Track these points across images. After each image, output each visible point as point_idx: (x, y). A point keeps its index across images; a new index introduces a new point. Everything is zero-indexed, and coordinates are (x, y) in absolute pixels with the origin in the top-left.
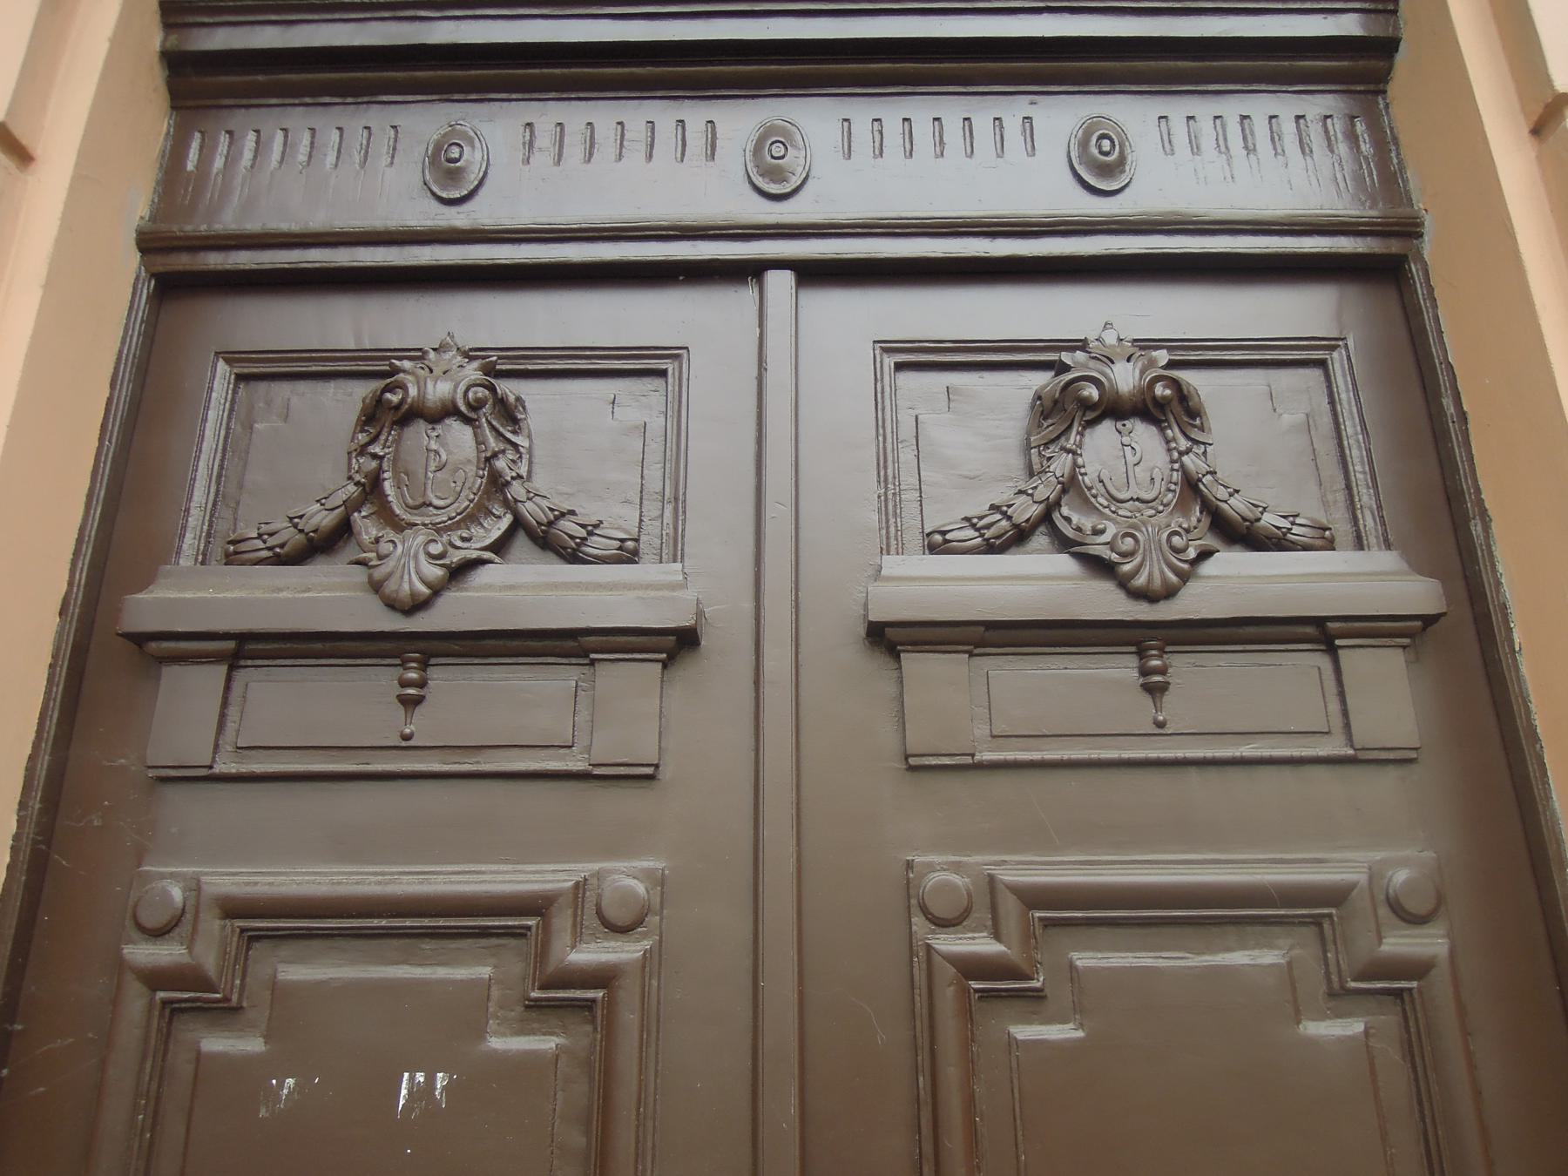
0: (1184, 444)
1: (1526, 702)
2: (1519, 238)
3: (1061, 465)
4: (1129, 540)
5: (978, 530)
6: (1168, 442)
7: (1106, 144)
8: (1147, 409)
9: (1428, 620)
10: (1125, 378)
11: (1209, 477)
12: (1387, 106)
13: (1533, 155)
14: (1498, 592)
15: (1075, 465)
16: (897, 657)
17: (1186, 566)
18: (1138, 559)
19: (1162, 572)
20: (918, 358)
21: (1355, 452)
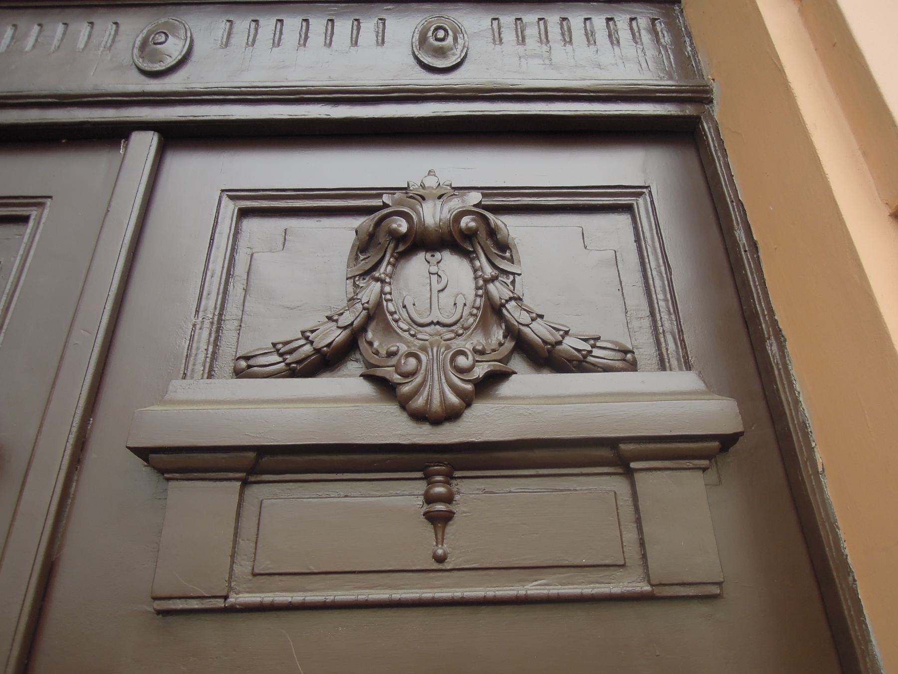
0: (489, 271)
1: (833, 528)
2: (788, 71)
3: (370, 292)
4: (412, 362)
5: (281, 355)
6: (475, 271)
7: (441, 34)
8: (452, 240)
9: (727, 442)
10: (432, 215)
11: (513, 303)
12: (682, 12)
13: (795, 9)
14: (797, 410)
15: (382, 292)
16: (633, 475)
17: (469, 387)
18: (418, 379)
19: (442, 393)
20: (258, 206)
21: (658, 283)
